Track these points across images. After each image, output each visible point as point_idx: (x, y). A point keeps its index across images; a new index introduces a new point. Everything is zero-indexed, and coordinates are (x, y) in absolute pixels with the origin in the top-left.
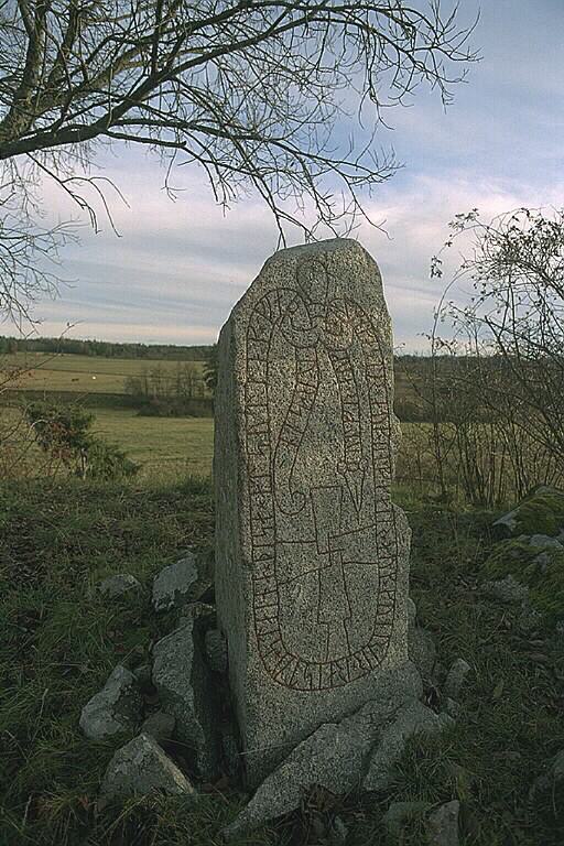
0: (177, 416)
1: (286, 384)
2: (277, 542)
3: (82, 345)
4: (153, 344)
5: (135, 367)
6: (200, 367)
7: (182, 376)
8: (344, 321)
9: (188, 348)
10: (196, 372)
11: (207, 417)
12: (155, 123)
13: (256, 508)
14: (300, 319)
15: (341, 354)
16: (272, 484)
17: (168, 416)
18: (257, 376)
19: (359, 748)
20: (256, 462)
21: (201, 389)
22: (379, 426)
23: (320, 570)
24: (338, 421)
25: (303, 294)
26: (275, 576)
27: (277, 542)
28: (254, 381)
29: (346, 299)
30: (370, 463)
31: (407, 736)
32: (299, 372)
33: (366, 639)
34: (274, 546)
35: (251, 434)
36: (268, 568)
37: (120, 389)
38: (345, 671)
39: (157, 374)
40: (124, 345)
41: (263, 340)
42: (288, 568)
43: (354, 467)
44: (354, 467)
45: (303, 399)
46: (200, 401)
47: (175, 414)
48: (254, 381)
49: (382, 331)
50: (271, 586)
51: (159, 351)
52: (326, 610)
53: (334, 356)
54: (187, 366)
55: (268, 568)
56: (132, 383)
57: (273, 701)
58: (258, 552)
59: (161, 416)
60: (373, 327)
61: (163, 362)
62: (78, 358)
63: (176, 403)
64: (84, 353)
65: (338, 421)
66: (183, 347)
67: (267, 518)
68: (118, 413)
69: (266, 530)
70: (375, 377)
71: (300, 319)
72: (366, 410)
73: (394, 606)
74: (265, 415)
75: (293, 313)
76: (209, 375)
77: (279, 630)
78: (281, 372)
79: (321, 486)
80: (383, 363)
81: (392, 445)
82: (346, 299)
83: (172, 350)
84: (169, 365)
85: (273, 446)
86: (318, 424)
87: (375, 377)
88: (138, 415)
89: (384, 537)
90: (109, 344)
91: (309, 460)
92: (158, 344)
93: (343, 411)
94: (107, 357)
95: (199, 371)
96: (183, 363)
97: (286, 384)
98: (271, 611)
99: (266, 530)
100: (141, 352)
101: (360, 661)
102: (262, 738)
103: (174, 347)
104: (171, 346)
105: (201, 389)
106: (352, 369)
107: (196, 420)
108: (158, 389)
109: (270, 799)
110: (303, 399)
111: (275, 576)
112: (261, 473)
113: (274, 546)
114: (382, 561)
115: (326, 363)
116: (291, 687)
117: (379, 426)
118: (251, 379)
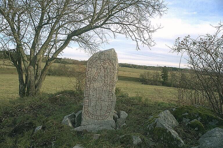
0: (152, 85)
1: (94, 72)
3: (131, 65)
4: (148, 66)
5: (142, 71)
6: (160, 72)
7: (155, 74)
10: (158, 74)
12: (113, 23)
15: (105, 68)
18: (90, 70)
21: (160, 78)
25: (100, 59)
29: (108, 59)
37: (138, 77)
39: (148, 73)
40: (141, 66)
46: (159, 81)
47: (152, 84)
49: (114, 64)
51: (150, 68)
56: (141, 75)
62: (130, 68)
64: (131, 67)
68: (136, 83)
76: (162, 75)
81: (114, 83)
82: (108, 59)
83: (154, 68)
84: (152, 71)
88: (142, 84)
90: (137, 65)
92: (150, 66)
94: (136, 68)
96: (155, 71)
97: (94, 72)
100: (145, 68)
102: (83, 123)
103: (154, 67)
106: (107, 70)
108: (148, 77)
109: (78, 129)
118: (88, 70)
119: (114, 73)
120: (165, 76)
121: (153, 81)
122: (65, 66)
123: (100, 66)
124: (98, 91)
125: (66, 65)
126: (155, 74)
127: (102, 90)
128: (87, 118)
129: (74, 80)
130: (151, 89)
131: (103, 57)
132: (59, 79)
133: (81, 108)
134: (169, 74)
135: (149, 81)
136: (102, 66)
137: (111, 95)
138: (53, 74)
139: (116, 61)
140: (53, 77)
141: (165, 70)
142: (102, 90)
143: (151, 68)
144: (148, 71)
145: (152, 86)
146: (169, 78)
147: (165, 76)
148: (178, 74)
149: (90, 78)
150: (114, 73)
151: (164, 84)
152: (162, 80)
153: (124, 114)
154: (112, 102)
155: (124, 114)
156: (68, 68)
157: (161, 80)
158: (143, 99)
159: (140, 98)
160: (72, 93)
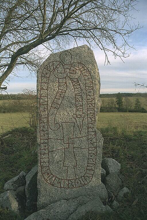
0: (108, 112)
1: (54, 90)
2: (48, 139)
6: (115, 99)
7: (109, 102)
8: (77, 70)
9: (112, 94)
11: (117, 112)
13: (42, 128)
14: (60, 69)
15: (75, 80)
16: (48, 121)
17: (106, 112)
18: (44, 88)
19: (69, 210)
20: (42, 113)
21: (115, 105)
22: (90, 103)
23: (64, 149)
24: (73, 101)
25: (62, 62)
26: (48, 149)
27: (48, 139)
28: (43, 89)
29: (79, 63)
30: (86, 115)
31: (88, 211)
32: (59, 86)
33: (82, 174)
34: (48, 139)
35: (41, 105)
36: (45, 146)
38: (73, 184)
41: (46, 77)
42: (53, 148)
43: (79, 116)
44: (79, 116)
45: (60, 95)
47: (108, 112)
48: (43, 89)
49: (92, 72)
50: (46, 152)
51: (104, 95)
52: (66, 162)
53: (72, 81)
54: (111, 99)
55: (45, 146)
57: (46, 190)
58: (42, 141)
59: (104, 112)
60: (89, 71)
61: (104, 98)
63: (108, 109)
65: (73, 101)
66: (111, 94)
67: (45, 131)
69: (45, 135)
70: (89, 87)
71: (60, 69)
72: (84, 97)
73: (95, 164)
74: (46, 99)
75: (58, 68)
76: (117, 101)
77: (49, 166)
78: (53, 86)
79: (66, 122)
80: (92, 82)
81: (96, 109)
85: (49, 109)
86: (65, 102)
87: (89, 87)
89: (91, 140)
91: (61, 113)
92: (104, 94)
93: (76, 98)
95: (114, 100)
96: (110, 98)
97: (54, 90)
98: (46, 160)
99: (45, 135)
101: (80, 181)
102: (42, 200)
103: (108, 94)
104: (107, 94)
105: (115, 105)
107: (113, 113)
108: (103, 105)
110: (60, 95)
111: (48, 149)
112: (44, 117)
113: (48, 139)
114: (90, 148)
115: (69, 83)
116: (53, 185)
117: (90, 103)
119: (93, 89)
120: (119, 103)
121: (108, 107)
122: (19, 101)
123: (65, 78)
124: (65, 130)
125: (21, 101)
126: (109, 102)
127: (74, 126)
128: (49, 187)
129: (27, 115)
130: (109, 116)
131: (68, 59)
132: (15, 115)
133: (34, 162)
134: (124, 99)
135: (105, 109)
136: (68, 79)
137: (93, 133)
138: (8, 111)
139: (94, 66)
140: (9, 114)
141: (119, 96)
142: (74, 126)
143: (105, 95)
144: (103, 98)
145: (108, 113)
146: (123, 103)
147: (119, 103)
148: (133, 100)
149: (46, 103)
150: (93, 89)
151: (120, 110)
152: (117, 106)
153: (114, 165)
154: (96, 148)
155: (114, 165)
156: (22, 104)
157: (117, 106)
158: (119, 131)
159: (115, 129)
160: (24, 131)
